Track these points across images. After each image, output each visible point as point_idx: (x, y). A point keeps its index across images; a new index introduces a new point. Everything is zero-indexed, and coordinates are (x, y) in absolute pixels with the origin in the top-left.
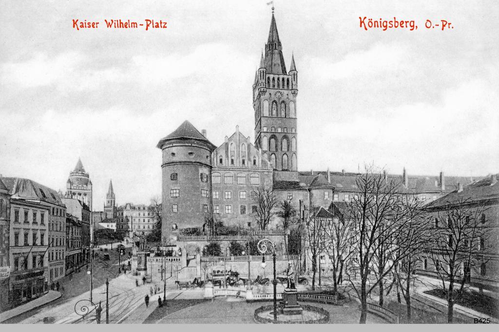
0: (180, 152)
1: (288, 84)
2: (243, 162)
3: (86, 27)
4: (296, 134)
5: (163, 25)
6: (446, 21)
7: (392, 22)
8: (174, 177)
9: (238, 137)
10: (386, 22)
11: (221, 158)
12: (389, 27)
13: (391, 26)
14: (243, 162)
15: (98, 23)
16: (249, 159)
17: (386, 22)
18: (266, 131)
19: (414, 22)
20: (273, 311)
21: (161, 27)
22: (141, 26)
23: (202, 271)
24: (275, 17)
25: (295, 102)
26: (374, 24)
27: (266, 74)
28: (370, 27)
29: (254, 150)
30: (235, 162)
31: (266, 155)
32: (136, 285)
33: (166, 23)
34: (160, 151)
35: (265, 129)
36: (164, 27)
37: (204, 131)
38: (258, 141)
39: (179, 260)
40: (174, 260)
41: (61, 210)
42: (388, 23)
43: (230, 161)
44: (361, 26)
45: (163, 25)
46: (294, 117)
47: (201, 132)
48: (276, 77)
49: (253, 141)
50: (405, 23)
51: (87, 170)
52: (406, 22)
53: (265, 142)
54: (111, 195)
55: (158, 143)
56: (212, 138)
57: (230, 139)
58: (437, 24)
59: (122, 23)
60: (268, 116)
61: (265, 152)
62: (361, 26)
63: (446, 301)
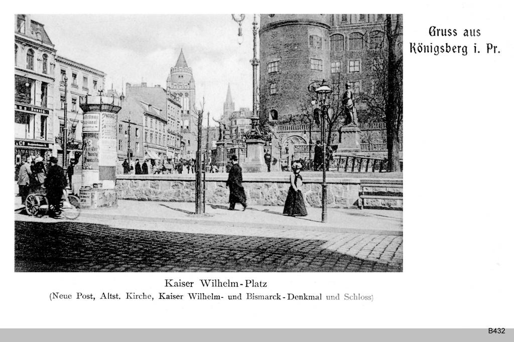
3: (446, 35)
6: (265, 157)
10: (447, 51)
13: (499, 332)
15: (151, 105)
17: (447, 51)
19: (466, 47)
22: (190, 142)
26: (366, 298)
27: (321, 131)
28: (420, 52)
32: (267, 170)
42: (445, 50)
44: (411, 51)
45: (262, 285)
50: (457, 48)
52: (459, 47)
58: (243, 32)
59: (449, 46)
62: (411, 51)
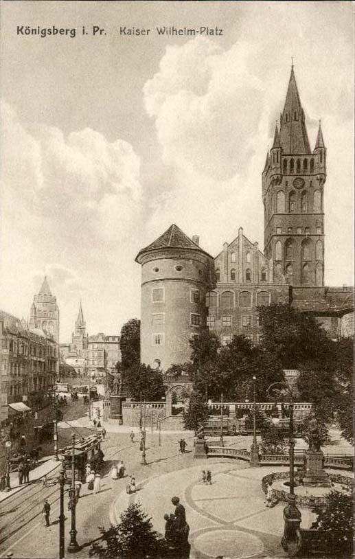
0: (166, 265)
1: (292, 166)
4: (323, 234)
5: (218, 32)
8: (157, 295)
9: (240, 244)
18: (280, 233)
20: (288, 480)
21: (217, 34)
24: (295, 74)
25: (321, 190)
31: (279, 266)
35: (279, 232)
36: (220, 34)
38: (268, 248)
39: (163, 406)
40: (156, 406)
43: (230, 276)
45: (218, 32)
46: (319, 212)
48: (289, 158)
49: (261, 247)
53: (279, 247)
54: (81, 328)
60: (284, 213)
63: (118, 140)
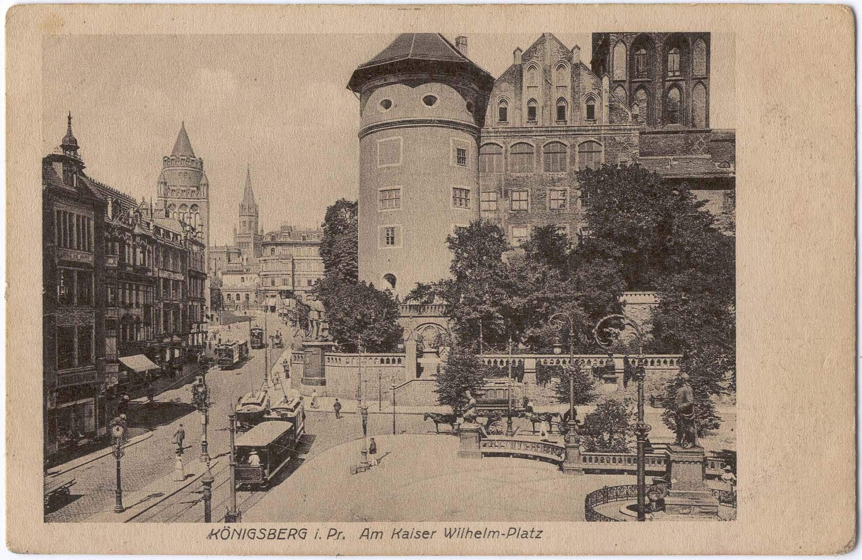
2: (561, 112)
7: (415, 537)
11: (503, 105)
12: (415, 537)
13: (417, 536)
14: (561, 112)
16: (577, 107)
23: (273, 361)
29: (587, 81)
30: (539, 112)
31: (620, 92)
33: (541, 532)
34: (353, 99)
37: (461, 41)
39: (399, 361)
41: (78, 216)
47: (454, 43)
51: (200, 149)
54: (249, 211)
55: (349, 78)
56: (477, 56)
57: (528, 55)
61: (619, 83)
